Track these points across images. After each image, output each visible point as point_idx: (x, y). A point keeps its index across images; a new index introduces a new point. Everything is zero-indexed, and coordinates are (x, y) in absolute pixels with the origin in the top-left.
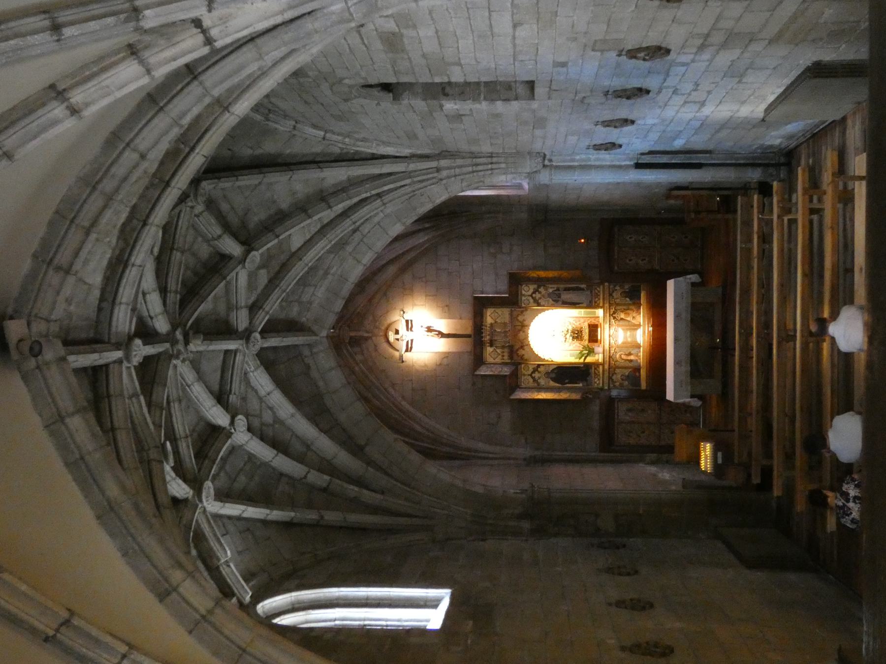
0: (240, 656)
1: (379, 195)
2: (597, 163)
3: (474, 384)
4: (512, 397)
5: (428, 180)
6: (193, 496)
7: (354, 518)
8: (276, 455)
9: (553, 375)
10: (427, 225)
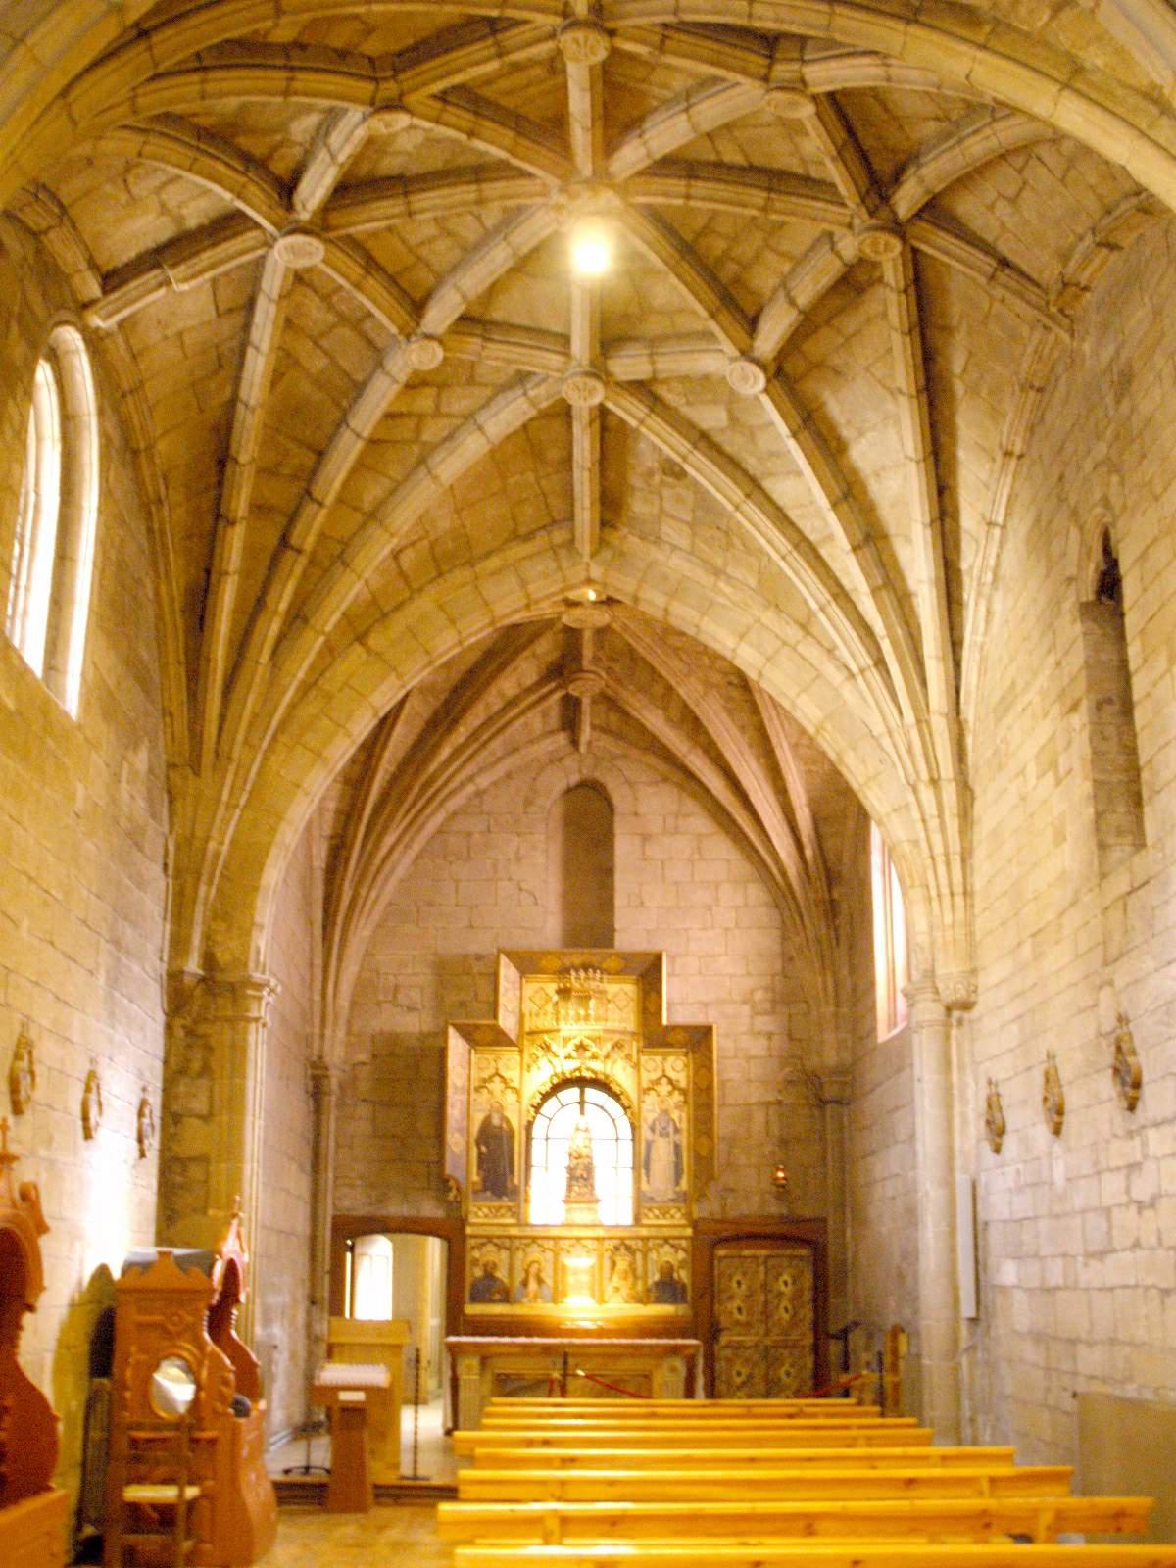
0: (10, 35)
1: (880, 663)
2: (957, 1122)
3: (479, 958)
4: (451, 1031)
6: (297, 221)
7: (228, 597)
9: (496, 1121)
10: (809, 853)
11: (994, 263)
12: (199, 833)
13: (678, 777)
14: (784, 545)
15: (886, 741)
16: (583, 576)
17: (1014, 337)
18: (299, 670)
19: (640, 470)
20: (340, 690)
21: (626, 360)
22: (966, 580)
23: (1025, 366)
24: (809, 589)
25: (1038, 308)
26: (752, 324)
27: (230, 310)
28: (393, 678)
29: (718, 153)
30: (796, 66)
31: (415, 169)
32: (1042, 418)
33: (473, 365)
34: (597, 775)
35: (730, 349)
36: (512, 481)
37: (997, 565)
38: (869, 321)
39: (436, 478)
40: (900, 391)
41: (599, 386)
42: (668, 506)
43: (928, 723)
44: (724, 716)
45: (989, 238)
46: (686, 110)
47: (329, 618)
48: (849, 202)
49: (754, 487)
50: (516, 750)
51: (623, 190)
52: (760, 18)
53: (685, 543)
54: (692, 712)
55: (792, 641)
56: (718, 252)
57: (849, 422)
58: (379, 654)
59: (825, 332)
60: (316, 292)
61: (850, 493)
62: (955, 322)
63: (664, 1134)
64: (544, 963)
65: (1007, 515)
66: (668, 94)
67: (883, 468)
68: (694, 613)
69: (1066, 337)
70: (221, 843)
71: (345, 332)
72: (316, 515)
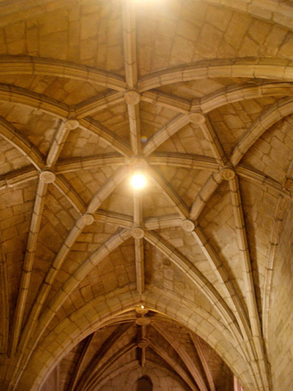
1: (235, 321)
5: (248, 354)
6: (47, 168)
11: (264, 177)
12: (7, 378)
13: (172, 374)
14: (202, 284)
15: (239, 349)
16: (139, 300)
17: (271, 203)
18: (47, 322)
19: (157, 264)
20: (61, 333)
21: (151, 223)
22: (262, 290)
23: (276, 212)
24: (211, 298)
25: (279, 189)
26: (189, 209)
27: (28, 201)
28: (78, 329)
29: (177, 149)
30: (198, 106)
31: (84, 155)
32: (283, 230)
33: (104, 224)
34: (147, 374)
35: (183, 217)
36: (117, 267)
37: (272, 283)
38: (226, 206)
39: (92, 263)
40: (237, 228)
41: (142, 231)
42: (166, 276)
43: (252, 340)
44: (186, 353)
45: (262, 170)
46: (166, 129)
47: (57, 307)
48: (218, 161)
49: (192, 266)
50: (122, 366)
51: (148, 159)
52: (186, 77)
53: (171, 288)
54: (176, 352)
55: (206, 318)
56: (178, 185)
57: (221, 241)
58: (74, 322)
59: (213, 211)
60: (55, 198)
61: (223, 265)
62: (253, 203)
65: (274, 265)
66: (160, 126)
67: (233, 256)
68: (174, 310)
69: (289, 197)
70: (15, 383)
71: (64, 213)
72: (54, 272)
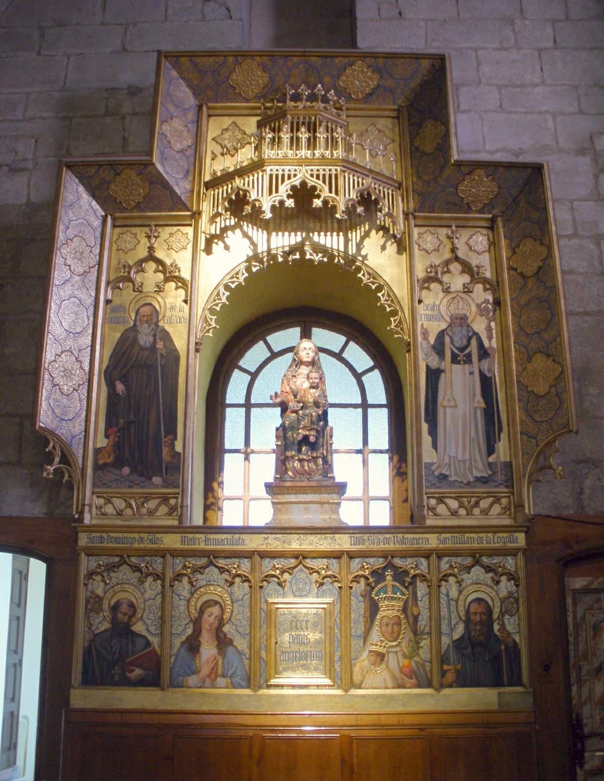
3: (134, 91)
8: (337, 451)
9: (144, 339)
63: (461, 357)
64: (237, 77)
